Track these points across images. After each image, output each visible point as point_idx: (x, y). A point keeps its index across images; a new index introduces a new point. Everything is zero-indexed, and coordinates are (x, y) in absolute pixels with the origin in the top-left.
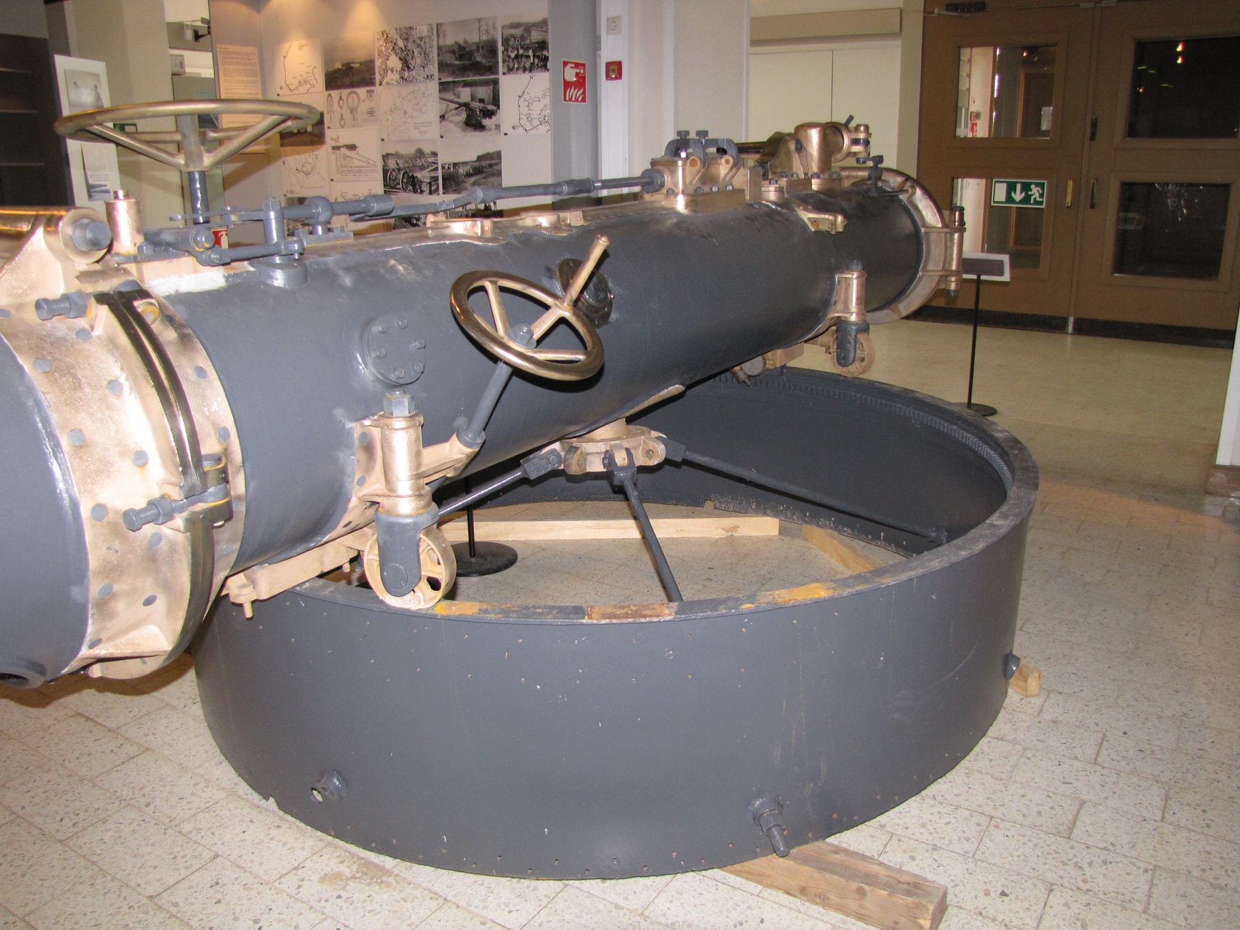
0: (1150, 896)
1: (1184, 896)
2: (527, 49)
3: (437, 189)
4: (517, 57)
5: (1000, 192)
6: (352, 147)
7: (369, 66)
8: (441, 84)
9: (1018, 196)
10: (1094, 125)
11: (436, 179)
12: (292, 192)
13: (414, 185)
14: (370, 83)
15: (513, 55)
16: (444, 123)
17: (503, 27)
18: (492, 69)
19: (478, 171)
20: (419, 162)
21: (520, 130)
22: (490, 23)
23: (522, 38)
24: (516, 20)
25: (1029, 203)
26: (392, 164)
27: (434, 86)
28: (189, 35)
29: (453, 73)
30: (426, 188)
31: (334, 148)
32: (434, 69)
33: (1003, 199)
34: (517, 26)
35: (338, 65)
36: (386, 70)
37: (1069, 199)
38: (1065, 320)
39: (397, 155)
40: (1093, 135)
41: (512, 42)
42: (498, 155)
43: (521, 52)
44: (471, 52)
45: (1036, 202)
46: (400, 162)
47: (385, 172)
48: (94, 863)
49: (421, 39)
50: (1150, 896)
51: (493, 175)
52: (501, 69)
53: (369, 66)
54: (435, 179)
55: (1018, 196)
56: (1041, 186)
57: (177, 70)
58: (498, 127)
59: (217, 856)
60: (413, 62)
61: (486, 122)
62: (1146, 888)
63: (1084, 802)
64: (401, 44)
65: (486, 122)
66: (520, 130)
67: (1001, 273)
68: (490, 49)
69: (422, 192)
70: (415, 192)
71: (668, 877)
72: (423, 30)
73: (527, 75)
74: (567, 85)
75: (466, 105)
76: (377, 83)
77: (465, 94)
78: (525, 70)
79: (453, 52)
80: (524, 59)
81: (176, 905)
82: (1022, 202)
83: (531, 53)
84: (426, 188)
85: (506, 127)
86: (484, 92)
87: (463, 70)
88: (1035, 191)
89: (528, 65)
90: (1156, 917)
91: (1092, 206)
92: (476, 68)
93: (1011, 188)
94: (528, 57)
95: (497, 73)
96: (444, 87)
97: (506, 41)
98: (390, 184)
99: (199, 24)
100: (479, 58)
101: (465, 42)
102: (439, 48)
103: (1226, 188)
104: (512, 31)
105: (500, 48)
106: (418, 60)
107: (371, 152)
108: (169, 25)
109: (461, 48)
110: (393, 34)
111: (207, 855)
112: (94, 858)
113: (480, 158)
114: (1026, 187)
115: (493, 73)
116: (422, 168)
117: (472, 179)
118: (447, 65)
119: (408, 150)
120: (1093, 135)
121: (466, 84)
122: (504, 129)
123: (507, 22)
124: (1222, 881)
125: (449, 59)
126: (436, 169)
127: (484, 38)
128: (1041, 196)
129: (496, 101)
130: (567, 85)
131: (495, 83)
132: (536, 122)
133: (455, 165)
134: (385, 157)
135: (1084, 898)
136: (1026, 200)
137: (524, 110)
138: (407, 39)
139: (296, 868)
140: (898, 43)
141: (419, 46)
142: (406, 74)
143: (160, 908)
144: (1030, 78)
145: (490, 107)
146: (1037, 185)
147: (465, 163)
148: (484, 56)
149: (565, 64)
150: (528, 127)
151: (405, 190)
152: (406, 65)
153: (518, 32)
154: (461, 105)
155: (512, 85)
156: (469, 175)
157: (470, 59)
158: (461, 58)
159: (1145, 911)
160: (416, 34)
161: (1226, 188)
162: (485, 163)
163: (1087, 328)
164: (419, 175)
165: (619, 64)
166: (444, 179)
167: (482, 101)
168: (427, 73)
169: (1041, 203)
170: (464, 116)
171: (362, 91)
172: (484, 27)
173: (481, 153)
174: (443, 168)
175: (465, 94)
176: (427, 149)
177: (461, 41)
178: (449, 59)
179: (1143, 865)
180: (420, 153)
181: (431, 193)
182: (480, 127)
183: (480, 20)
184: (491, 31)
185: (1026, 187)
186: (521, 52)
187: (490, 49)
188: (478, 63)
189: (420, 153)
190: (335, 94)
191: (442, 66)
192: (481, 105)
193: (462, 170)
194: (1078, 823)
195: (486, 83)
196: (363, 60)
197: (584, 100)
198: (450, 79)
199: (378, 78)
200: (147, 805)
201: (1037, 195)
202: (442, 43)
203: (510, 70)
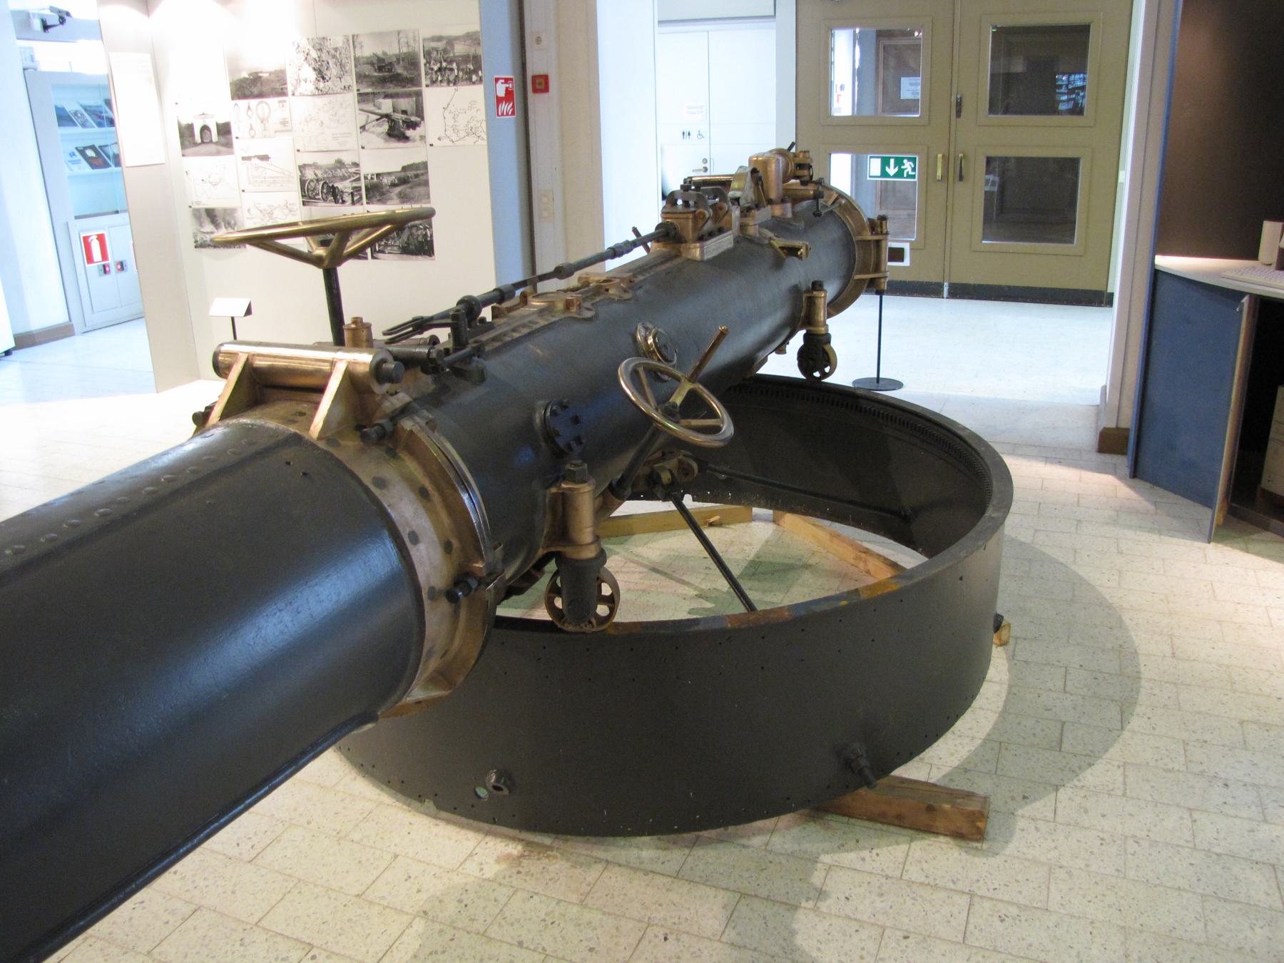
0: (1125, 783)
1: (255, 834)
2: (451, 62)
3: (361, 198)
4: (440, 69)
5: (874, 166)
6: (265, 158)
7: (280, 77)
8: (360, 95)
9: (892, 170)
10: (959, 104)
11: (359, 189)
12: (198, 203)
13: (335, 195)
14: (282, 93)
15: (436, 68)
16: (365, 134)
17: (424, 40)
18: (414, 81)
19: (403, 181)
20: (340, 173)
21: (446, 142)
22: (411, 35)
23: (445, 51)
24: (437, 33)
25: (902, 176)
26: (310, 175)
27: (352, 97)
28: (37, 25)
29: (373, 84)
30: (348, 198)
31: (244, 158)
32: (351, 80)
33: (878, 174)
34: (439, 39)
35: (245, 75)
36: (298, 81)
37: (939, 173)
38: (941, 286)
39: (315, 166)
40: (959, 114)
41: (434, 54)
42: (425, 165)
43: (444, 64)
44: (391, 64)
45: (909, 176)
46: (320, 173)
47: (303, 183)
48: (290, 876)
49: (336, 50)
50: (1125, 783)
51: (419, 185)
52: (424, 81)
53: (280, 77)
54: (358, 189)
55: (892, 170)
56: (913, 160)
57: (28, 64)
58: (423, 138)
59: (396, 856)
60: (328, 73)
61: (409, 133)
62: (1121, 779)
63: (1064, 723)
64: (314, 54)
65: (409, 133)
66: (446, 142)
67: (902, 260)
68: (412, 62)
69: (344, 202)
70: (336, 201)
71: (775, 819)
72: (338, 41)
73: (452, 88)
74: (499, 100)
75: (387, 116)
76: (290, 93)
77: (386, 106)
78: (449, 82)
79: (372, 64)
80: (448, 72)
81: (383, 898)
82: (896, 176)
83: (454, 66)
84: (348, 198)
85: (431, 138)
86: (405, 103)
87: (383, 81)
88: (908, 166)
89: (452, 78)
90: (1133, 798)
91: (961, 178)
92: (397, 79)
93: (885, 162)
94: (452, 70)
95: (419, 84)
96: (363, 97)
97: (428, 54)
98: (308, 196)
99: (48, 12)
100: (399, 70)
101: (384, 53)
102: (357, 60)
103: (1072, 164)
104: (434, 44)
105: (423, 61)
106: (333, 71)
107: (285, 165)
108: (15, 14)
109: (380, 60)
110: (306, 46)
111: (388, 857)
112: (288, 872)
113: (404, 169)
114: (899, 162)
115: (414, 85)
116: (343, 178)
117: (398, 190)
118: (365, 76)
119: (329, 160)
120: (959, 114)
121: (387, 96)
122: (430, 140)
123: (428, 35)
124: (1170, 767)
125: (368, 70)
126: (359, 179)
127: (405, 50)
128: (914, 169)
129: (420, 112)
130: (499, 100)
131: (419, 95)
132: (462, 134)
133: (378, 175)
134: (302, 168)
135: (1082, 793)
136: (900, 174)
137: (450, 121)
138: (320, 50)
139: (471, 855)
140: (772, 24)
141: (334, 57)
142: (321, 85)
143: (371, 903)
144: (889, 52)
145: (414, 119)
146: (909, 159)
147: (389, 174)
148: (405, 68)
149: (497, 80)
150: (454, 138)
151: (325, 200)
152: (321, 76)
153: (441, 45)
154: (383, 116)
155: (435, 98)
156: (393, 185)
157: (390, 71)
158: (380, 69)
159: (1124, 795)
160: (330, 45)
161: (1072, 164)
162: (410, 174)
163: (962, 291)
164: (340, 185)
165: (546, 77)
166: (367, 189)
167: (404, 112)
168: (344, 83)
169: (913, 177)
170: (386, 127)
171: (273, 102)
172: (403, 40)
173: (405, 164)
174: (366, 178)
175: (386, 106)
176: (347, 159)
177: (380, 53)
178: (368, 70)
179: (1116, 763)
180: (340, 164)
181: (353, 203)
182: (404, 138)
183: (399, 33)
184: (412, 43)
185: (899, 162)
186: (444, 64)
187: (412, 62)
188: (399, 75)
189: (340, 164)
190: (243, 103)
191: (361, 78)
192: (404, 117)
193: (386, 181)
194: (1065, 740)
195: (409, 95)
196: (272, 69)
197: (513, 113)
198: (370, 90)
199: (290, 88)
200: (309, 823)
201: (909, 169)
202: (359, 54)
203: (433, 82)
